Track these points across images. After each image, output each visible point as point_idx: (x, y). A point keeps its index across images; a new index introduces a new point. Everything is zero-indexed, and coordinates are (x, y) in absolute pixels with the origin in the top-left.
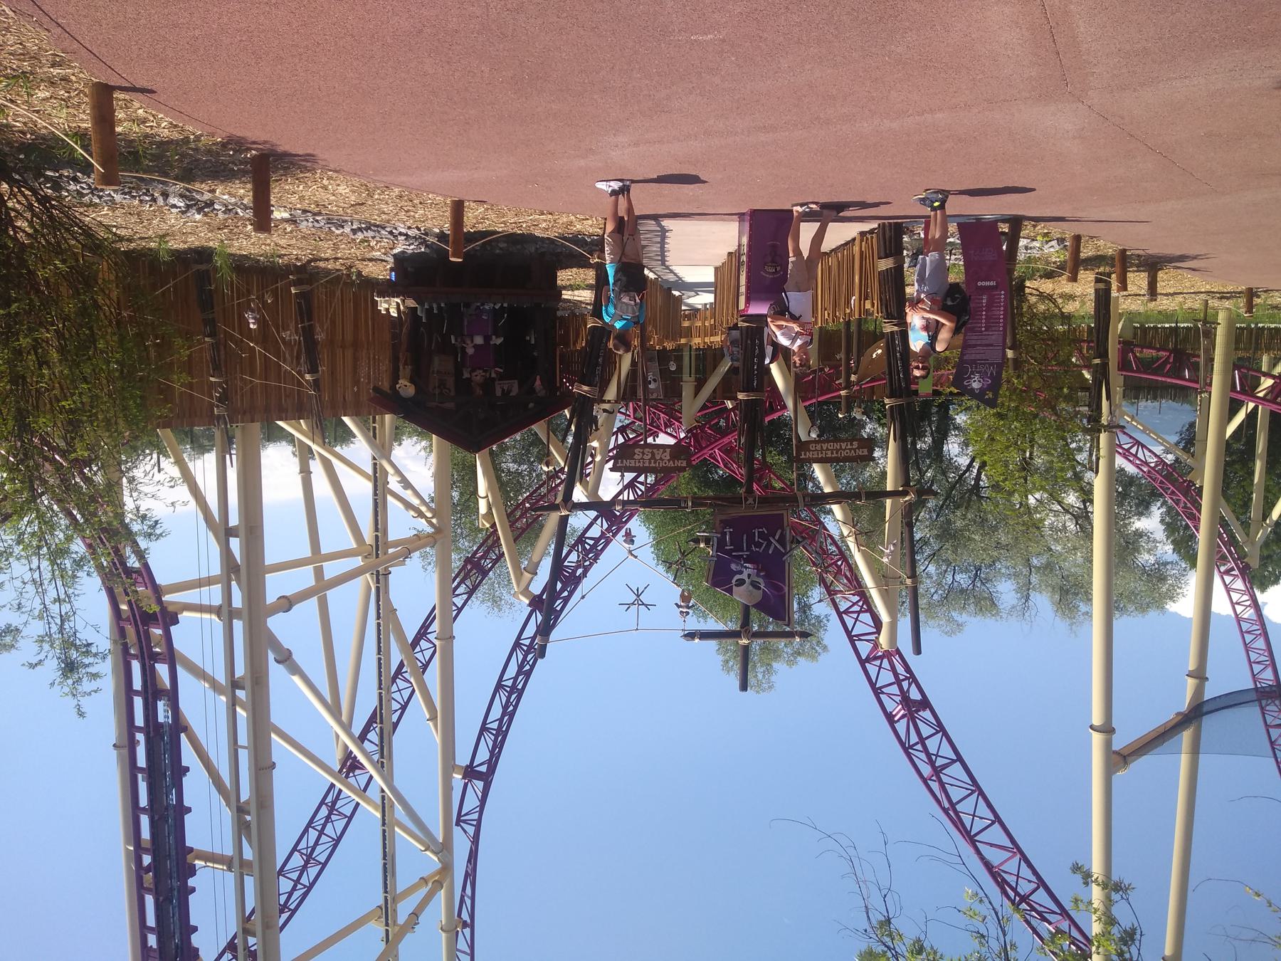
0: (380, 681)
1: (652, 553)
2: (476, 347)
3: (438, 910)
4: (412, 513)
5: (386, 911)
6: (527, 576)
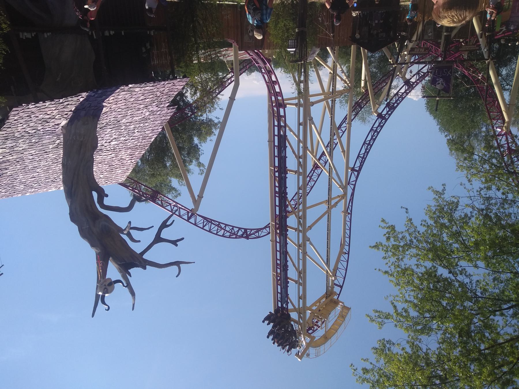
0: (331, 134)
1: (425, 107)
2: (376, 24)
3: (341, 205)
4: (343, 82)
5: (329, 201)
6: (377, 106)
